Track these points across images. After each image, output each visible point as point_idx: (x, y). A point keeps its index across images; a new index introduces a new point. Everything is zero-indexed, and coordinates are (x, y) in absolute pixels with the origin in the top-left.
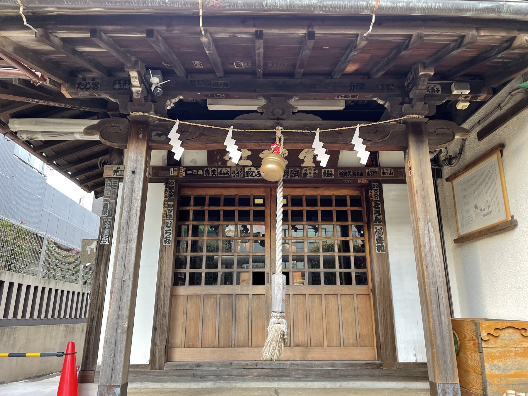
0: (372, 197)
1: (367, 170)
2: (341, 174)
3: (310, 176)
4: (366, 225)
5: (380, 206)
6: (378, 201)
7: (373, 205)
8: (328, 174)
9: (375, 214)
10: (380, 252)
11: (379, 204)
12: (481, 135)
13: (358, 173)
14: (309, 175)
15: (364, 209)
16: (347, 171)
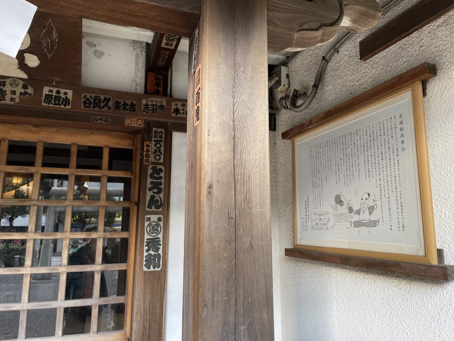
0: (148, 156)
1: (144, 102)
2: (87, 103)
3: (12, 99)
4: (135, 208)
5: (162, 175)
6: (160, 164)
7: (150, 171)
8: (58, 98)
9: (150, 189)
10: (152, 269)
11: (161, 170)
12: (368, 49)
13: (125, 104)
14: (8, 96)
15: (135, 177)
16: (102, 97)
